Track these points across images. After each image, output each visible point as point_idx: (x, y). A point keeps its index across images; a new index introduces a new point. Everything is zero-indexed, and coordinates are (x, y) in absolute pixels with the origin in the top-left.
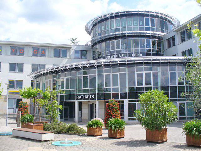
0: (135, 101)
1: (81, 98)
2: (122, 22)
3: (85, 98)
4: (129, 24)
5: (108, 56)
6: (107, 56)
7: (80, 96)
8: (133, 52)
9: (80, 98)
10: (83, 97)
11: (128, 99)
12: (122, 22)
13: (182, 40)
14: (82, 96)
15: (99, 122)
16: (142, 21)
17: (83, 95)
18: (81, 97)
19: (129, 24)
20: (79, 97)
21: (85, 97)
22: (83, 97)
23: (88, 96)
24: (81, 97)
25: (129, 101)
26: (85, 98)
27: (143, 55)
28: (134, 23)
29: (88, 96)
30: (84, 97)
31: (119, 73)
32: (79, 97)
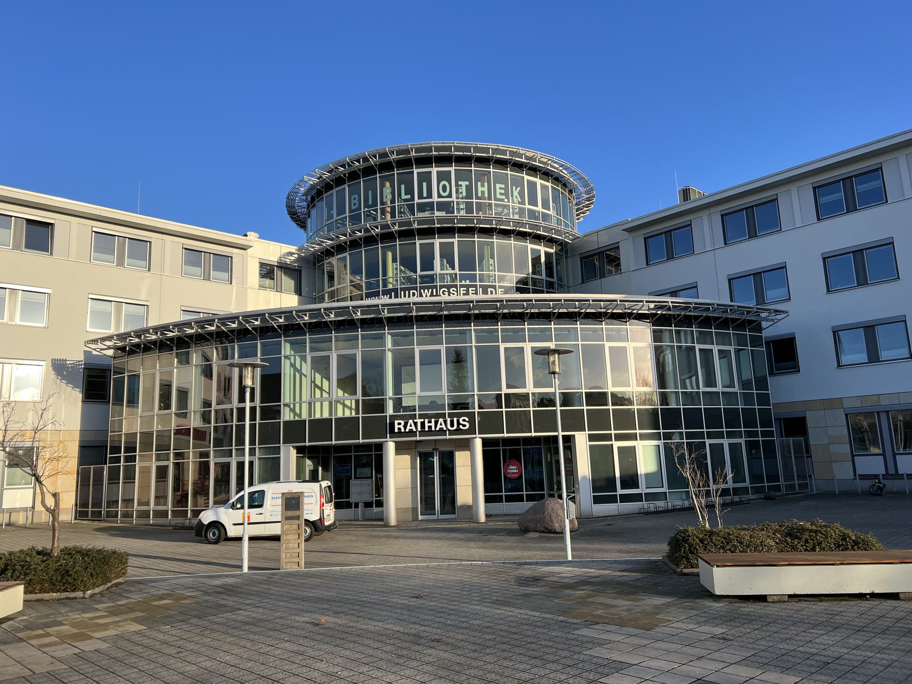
0: (608, 437)
1: (443, 426)
2: (460, 183)
3: (430, 427)
4: (483, 192)
5: (409, 289)
6: (404, 290)
7: (411, 421)
8: (497, 284)
9: (408, 428)
10: (423, 424)
11: (587, 432)
12: (460, 183)
13: (619, 248)
14: (419, 421)
15: (12, 624)
16: (519, 188)
17: (421, 416)
18: (415, 424)
19: (483, 192)
20: (405, 427)
21: (433, 424)
22: (423, 424)
23: (445, 422)
24: (415, 424)
25: (592, 438)
26: (430, 427)
27: (346, 269)
28: (498, 191)
29: (445, 422)
30: (427, 425)
31: (443, 348)
32: (405, 427)
